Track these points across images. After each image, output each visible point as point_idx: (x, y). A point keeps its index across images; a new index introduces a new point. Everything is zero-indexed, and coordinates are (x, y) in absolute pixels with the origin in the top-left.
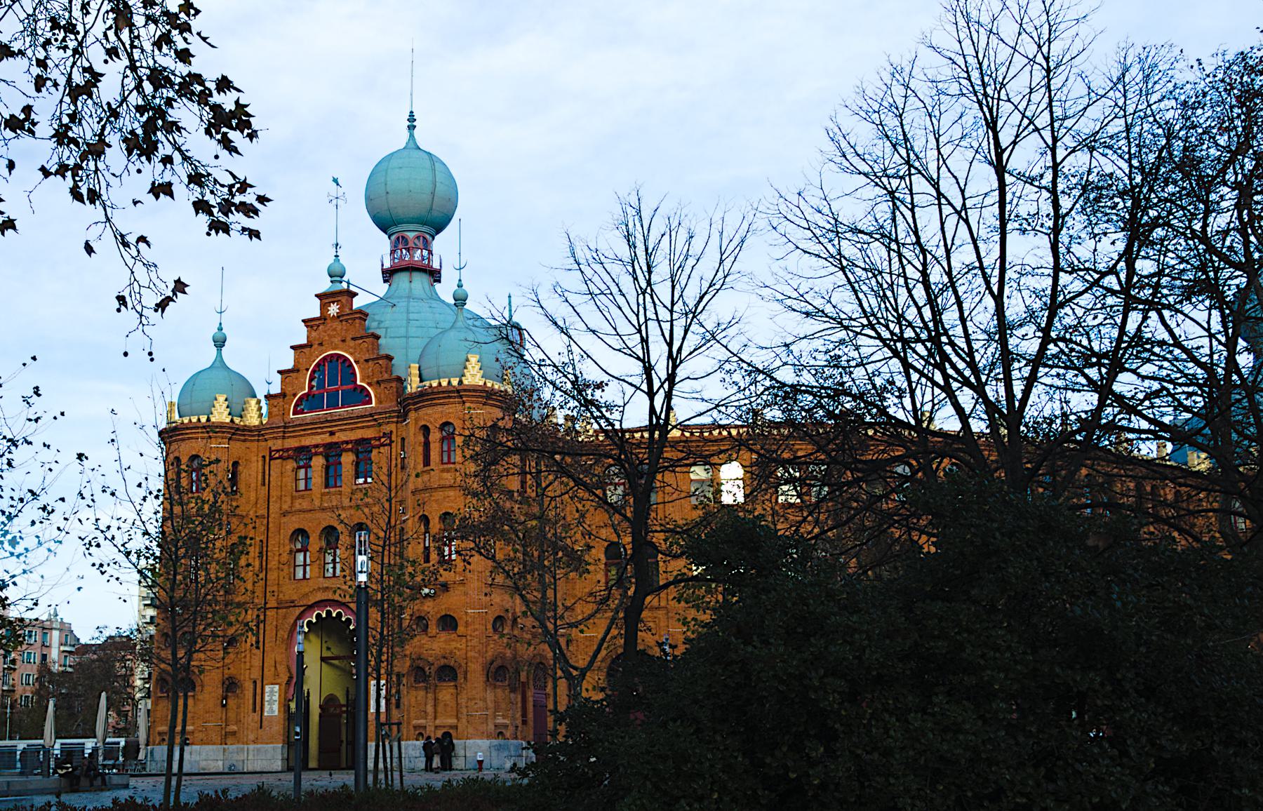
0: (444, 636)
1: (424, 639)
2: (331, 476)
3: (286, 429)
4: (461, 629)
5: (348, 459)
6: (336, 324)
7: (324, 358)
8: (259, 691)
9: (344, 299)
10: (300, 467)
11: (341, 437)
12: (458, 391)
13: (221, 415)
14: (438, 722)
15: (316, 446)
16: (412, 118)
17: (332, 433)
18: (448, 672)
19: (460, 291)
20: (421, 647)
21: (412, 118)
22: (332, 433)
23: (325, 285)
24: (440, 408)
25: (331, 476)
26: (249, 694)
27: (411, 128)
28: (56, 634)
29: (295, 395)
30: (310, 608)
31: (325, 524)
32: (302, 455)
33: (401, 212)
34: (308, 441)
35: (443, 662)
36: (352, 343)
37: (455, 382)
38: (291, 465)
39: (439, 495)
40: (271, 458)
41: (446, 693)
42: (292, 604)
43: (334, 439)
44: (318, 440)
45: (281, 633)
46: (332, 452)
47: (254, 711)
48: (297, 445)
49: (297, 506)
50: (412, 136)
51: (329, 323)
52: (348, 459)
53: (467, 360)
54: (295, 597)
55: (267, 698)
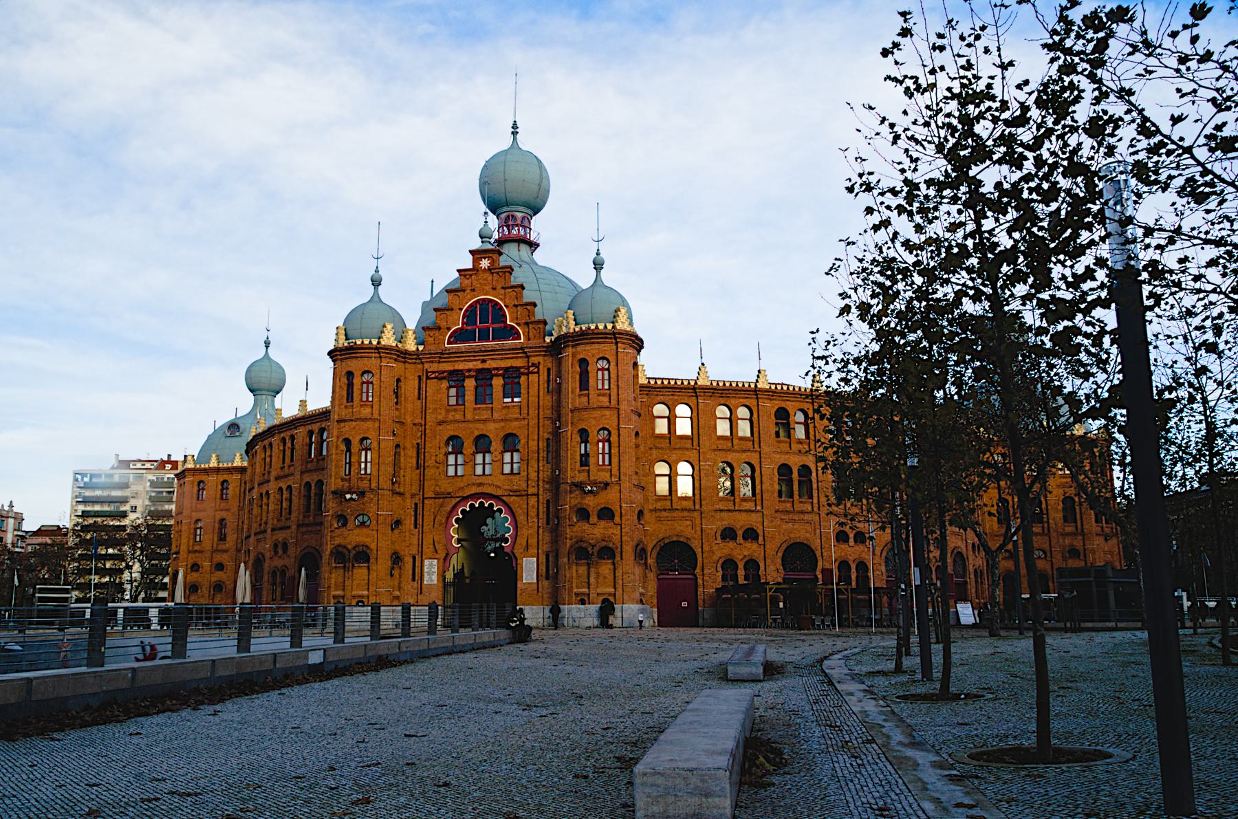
0: (603, 523)
1: (586, 526)
2: (483, 396)
3: (443, 355)
4: (617, 519)
5: (498, 382)
6: (488, 276)
7: (477, 302)
8: (418, 563)
9: (495, 256)
10: (451, 387)
11: (490, 364)
12: (614, 334)
13: (389, 340)
14: (599, 590)
15: (469, 370)
16: (515, 126)
17: (484, 361)
18: (608, 552)
19: (377, 276)
20: (584, 531)
21: (515, 126)
22: (484, 361)
23: (477, 244)
24: (596, 346)
25: (483, 396)
26: (409, 566)
27: (515, 133)
28: (11, 521)
29: (449, 329)
30: (465, 499)
31: (477, 433)
32: (456, 378)
33: (512, 195)
34: (460, 366)
35: (604, 544)
36: (502, 291)
37: (375, 342)
38: (445, 384)
39: (597, 413)
40: (428, 378)
41: (605, 568)
42: (448, 495)
43: (486, 366)
44: (470, 365)
45: (439, 517)
46: (483, 377)
47: (414, 580)
48: (451, 368)
49: (450, 417)
50: (515, 139)
51: (481, 275)
52: (498, 382)
53: (384, 326)
54: (450, 490)
55: (426, 570)
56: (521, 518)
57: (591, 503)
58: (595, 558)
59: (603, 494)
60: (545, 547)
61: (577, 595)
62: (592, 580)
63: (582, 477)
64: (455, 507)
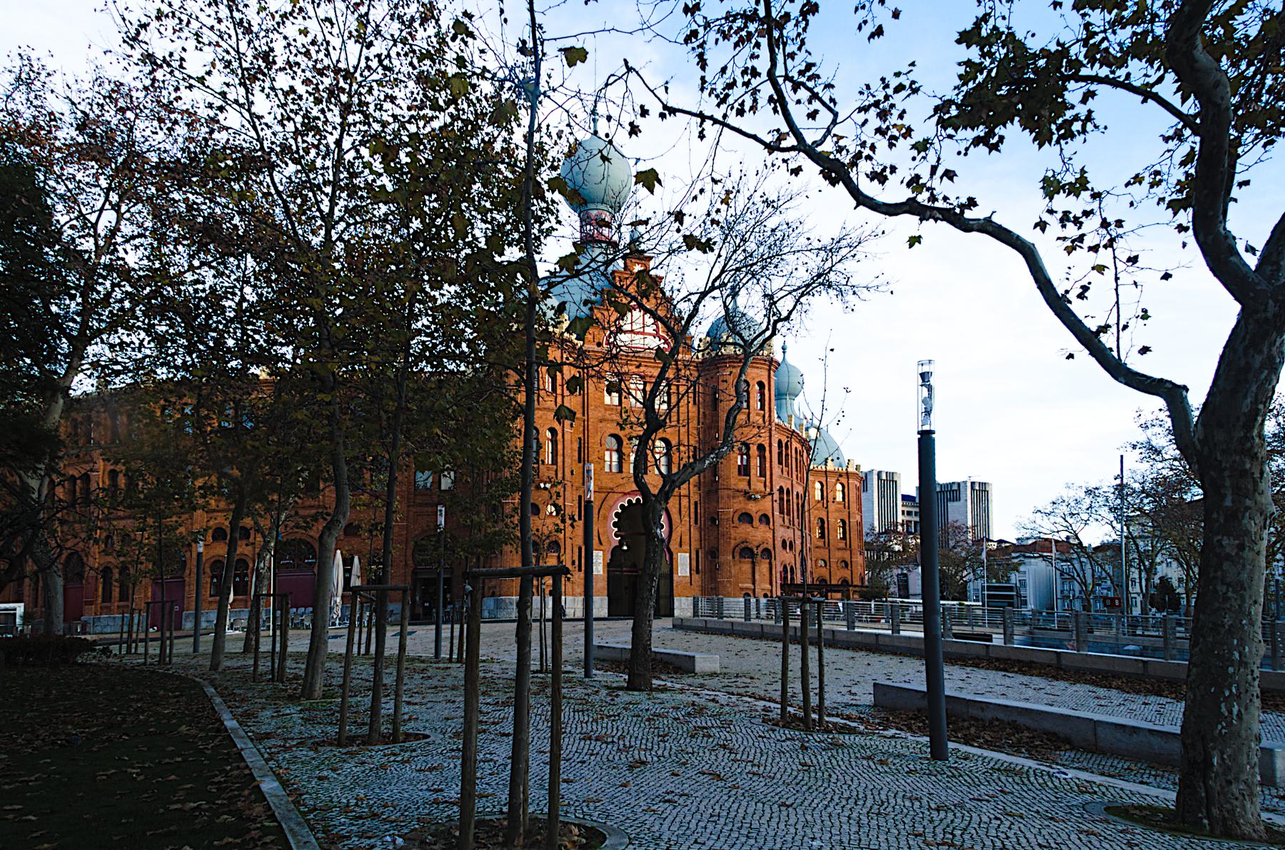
0: (763, 527)
35: (765, 546)
54: (611, 485)
56: (675, 517)
57: (752, 508)
58: (759, 557)
59: (762, 502)
60: (695, 545)
61: (742, 589)
62: (757, 577)
63: (743, 485)
64: (615, 503)
